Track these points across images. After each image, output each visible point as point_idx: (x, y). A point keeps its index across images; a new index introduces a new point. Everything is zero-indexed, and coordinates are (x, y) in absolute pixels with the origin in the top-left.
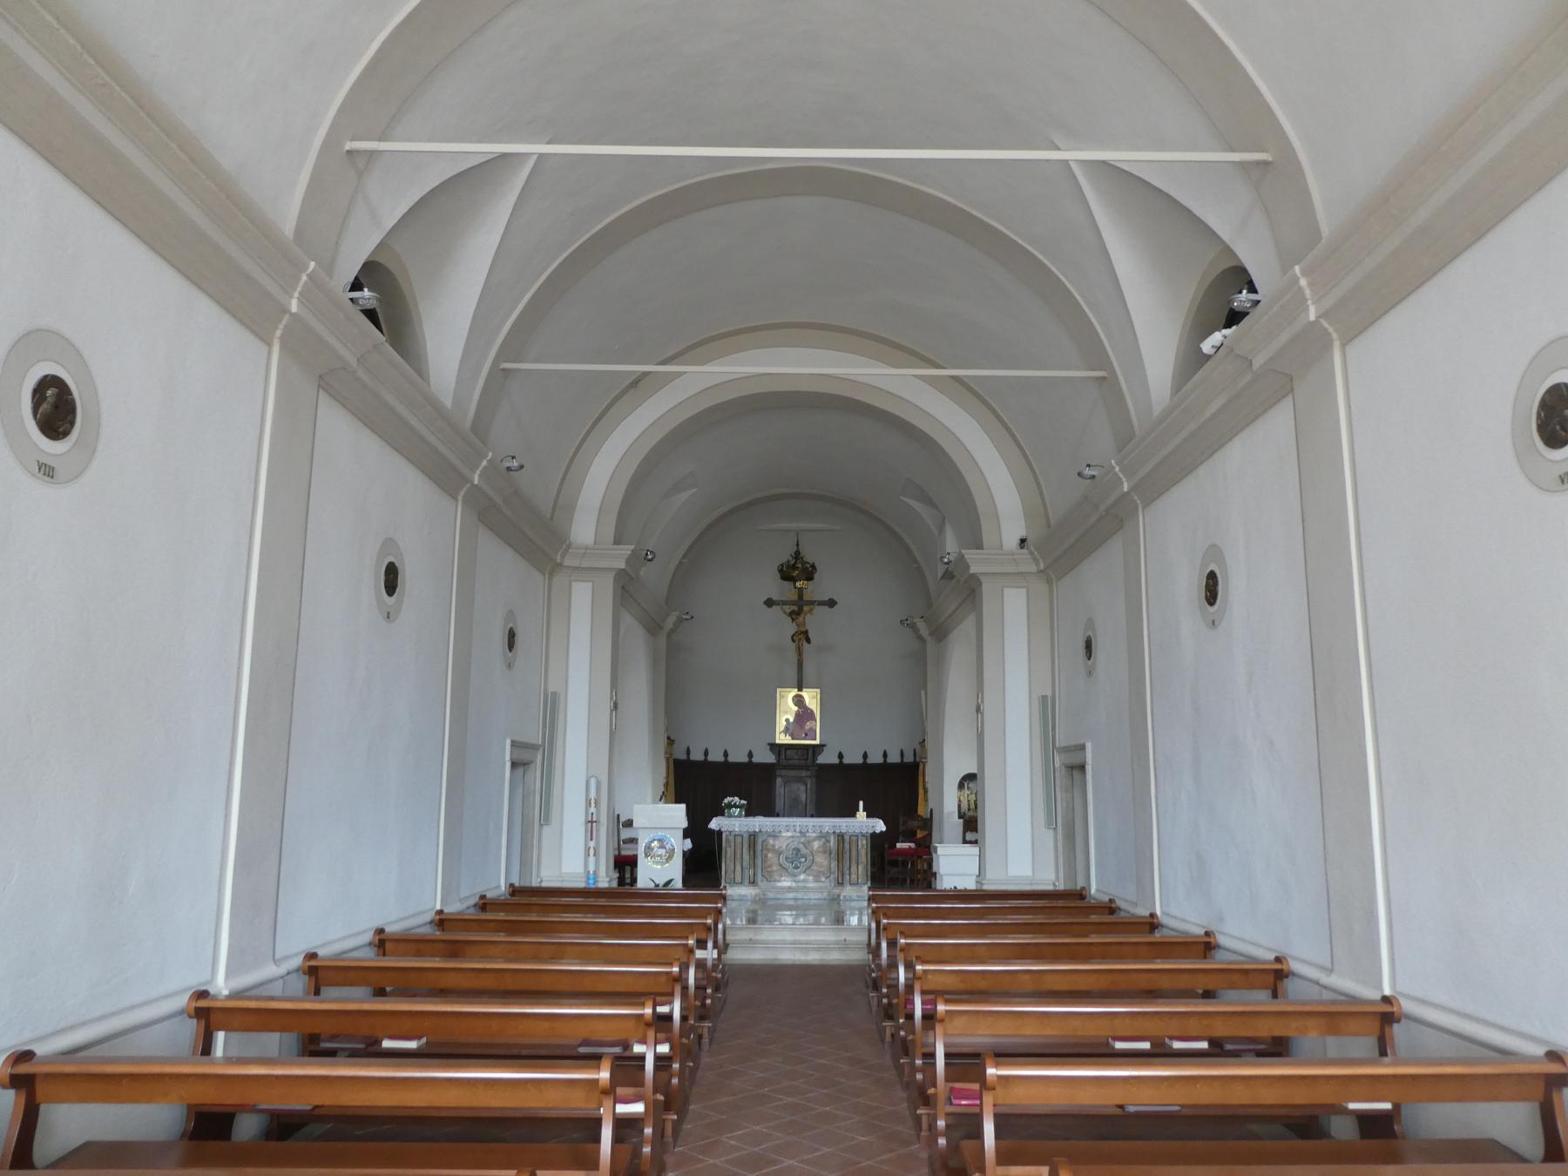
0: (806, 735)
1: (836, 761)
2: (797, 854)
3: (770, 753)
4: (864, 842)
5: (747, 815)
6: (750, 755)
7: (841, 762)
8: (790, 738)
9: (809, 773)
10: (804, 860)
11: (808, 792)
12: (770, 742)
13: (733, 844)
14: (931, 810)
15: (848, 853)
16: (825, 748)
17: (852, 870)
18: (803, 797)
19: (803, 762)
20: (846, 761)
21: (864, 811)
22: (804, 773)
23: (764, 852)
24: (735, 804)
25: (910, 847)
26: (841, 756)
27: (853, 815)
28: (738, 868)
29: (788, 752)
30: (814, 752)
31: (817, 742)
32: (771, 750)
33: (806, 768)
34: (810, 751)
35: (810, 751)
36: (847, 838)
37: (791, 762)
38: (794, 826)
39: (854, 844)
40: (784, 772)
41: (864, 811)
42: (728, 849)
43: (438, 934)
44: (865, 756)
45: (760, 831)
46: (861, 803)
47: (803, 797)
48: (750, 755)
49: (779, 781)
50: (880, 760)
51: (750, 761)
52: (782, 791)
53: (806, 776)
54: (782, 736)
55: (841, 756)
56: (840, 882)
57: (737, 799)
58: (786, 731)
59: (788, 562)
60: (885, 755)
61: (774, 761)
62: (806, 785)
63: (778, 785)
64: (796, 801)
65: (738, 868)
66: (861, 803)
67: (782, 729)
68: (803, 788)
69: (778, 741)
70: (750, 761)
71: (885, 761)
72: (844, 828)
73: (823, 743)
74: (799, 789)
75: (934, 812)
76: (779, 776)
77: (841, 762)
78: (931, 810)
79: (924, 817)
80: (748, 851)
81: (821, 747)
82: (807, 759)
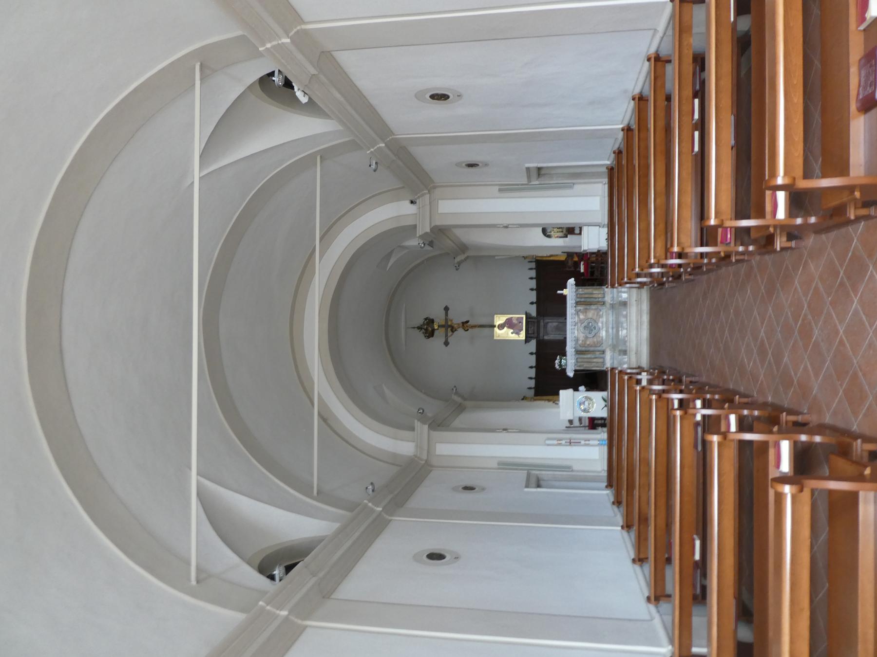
0: (520, 323)
1: (535, 306)
2: (587, 328)
6: (531, 354)
7: (535, 303)
8: (522, 332)
9: (542, 321)
10: (591, 324)
12: (524, 342)
19: (536, 325)
22: (542, 324)
23: (586, 346)
29: (530, 332)
31: (524, 316)
32: (528, 342)
33: (538, 322)
34: (529, 320)
35: (529, 320)
36: (578, 300)
40: (541, 335)
43: (635, 528)
44: (532, 290)
46: (559, 292)
47: (556, 324)
48: (531, 354)
49: (546, 338)
50: (534, 281)
53: (544, 322)
54: (520, 336)
55: (532, 303)
58: (518, 334)
60: (531, 278)
61: (535, 340)
62: (548, 322)
66: (559, 292)
67: (517, 336)
69: (524, 338)
81: (527, 314)
82: (534, 322)
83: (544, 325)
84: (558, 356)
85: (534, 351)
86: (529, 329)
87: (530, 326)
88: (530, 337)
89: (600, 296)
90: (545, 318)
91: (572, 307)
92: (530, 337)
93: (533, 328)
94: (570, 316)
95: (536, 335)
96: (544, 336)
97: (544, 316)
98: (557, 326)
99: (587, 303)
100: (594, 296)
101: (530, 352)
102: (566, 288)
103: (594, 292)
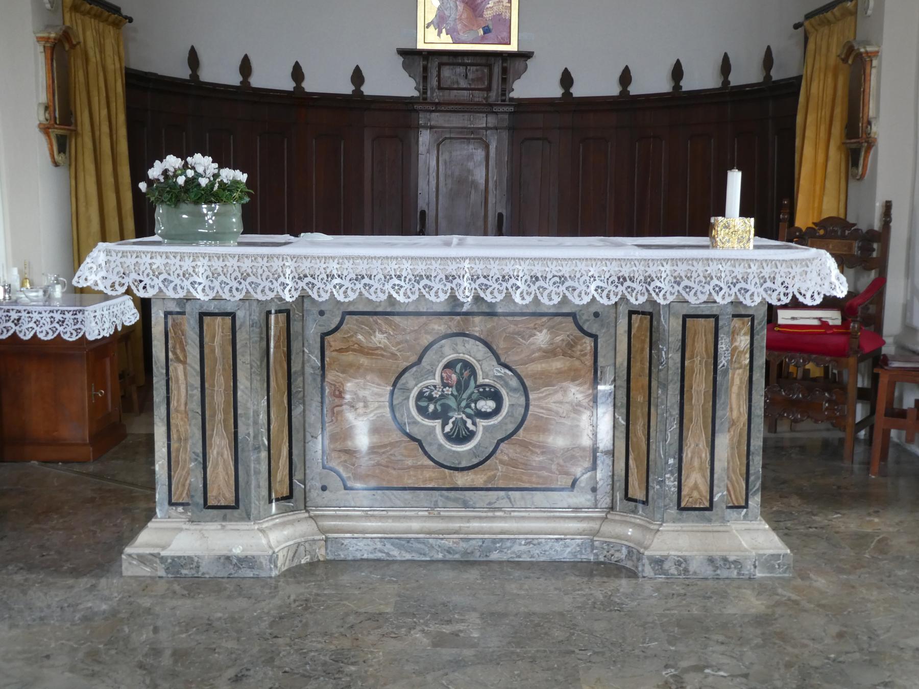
0: (487, 30)
1: (556, 92)
2: (461, 386)
3: (405, 74)
4: (743, 341)
5: (250, 226)
6: (358, 77)
7: (567, 94)
8: (448, 39)
9: (492, 120)
10: (487, 405)
11: (492, 162)
12: (407, 46)
13: (193, 352)
14: (888, 206)
15: (674, 389)
16: (529, 62)
17: (687, 454)
18: (479, 175)
19: (479, 97)
20: (578, 91)
21: (744, 213)
22: (481, 121)
23: (330, 376)
24: (192, 182)
25: (824, 324)
26: (567, 79)
27: (703, 228)
28: (220, 445)
29: (447, 72)
30: (505, 71)
31: (513, 47)
32: (406, 66)
33: (488, 108)
34: (497, 70)
35: (497, 70)
36: (672, 326)
37: (453, 95)
38: (450, 278)
39: (700, 346)
40: (437, 119)
41: (744, 213)
42: (178, 370)
43: (419, 211)
44: (626, 78)
45: (303, 298)
46: (735, 179)
47: (479, 175)
48: (358, 77)
49: (425, 138)
50: (663, 86)
51: (358, 92)
52: (433, 163)
53: (487, 128)
54: (432, 33)
55: (567, 79)
56: (636, 491)
57: (203, 163)
58: (440, 22)
59: (473, 175)
60: (677, 72)
61: (416, 94)
62: (487, 147)
63: (422, 149)
64: (463, 184)
65: (220, 445)
66: (735, 179)
67: (431, 17)
68: (480, 154)
69: (421, 46)
70: (358, 92)
71: (677, 87)
72: (666, 286)
73: (526, 49)
74: (470, 157)
75: (894, 212)
76: (426, 127)
77: (567, 94)
78: (888, 206)
79: (863, 227)
80: (260, 385)
81: (523, 56)
82: (489, 89)
83: (474, 131)
84: (243, 177)
85: (368, 89)
86: (461, 70)
87: (473, 72)
88: (425, 69)
89: (695, 479)
90: (505, 135)
91: (622, 280)
92: (425, 69)
93: (463, 84)
94: (553, 268)
95: (436, 96)
96: (431, 128)
97: (512, 129)
98: (474, 184)
99: (640, 382)
100: (696, 444)
101: (365, 73)
102: (760, 231)
103: (723, 442)
